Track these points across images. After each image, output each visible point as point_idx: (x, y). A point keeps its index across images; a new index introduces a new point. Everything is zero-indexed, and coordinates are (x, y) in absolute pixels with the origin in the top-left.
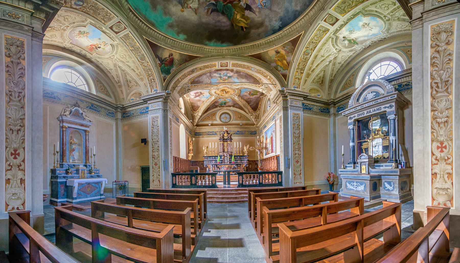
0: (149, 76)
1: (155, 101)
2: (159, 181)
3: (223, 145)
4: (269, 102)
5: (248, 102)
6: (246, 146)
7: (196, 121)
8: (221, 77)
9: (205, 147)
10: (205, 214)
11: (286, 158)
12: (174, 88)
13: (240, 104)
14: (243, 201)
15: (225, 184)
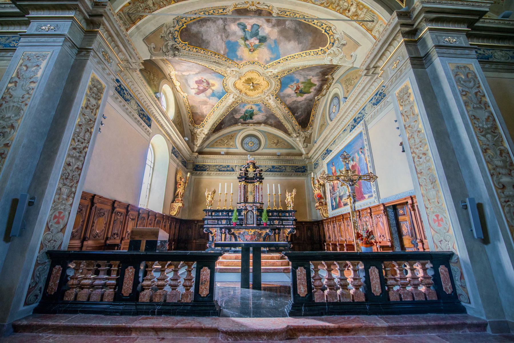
1: (53, 14)
6: (291, 191)
7: (199, 142)
15: (245, 284)
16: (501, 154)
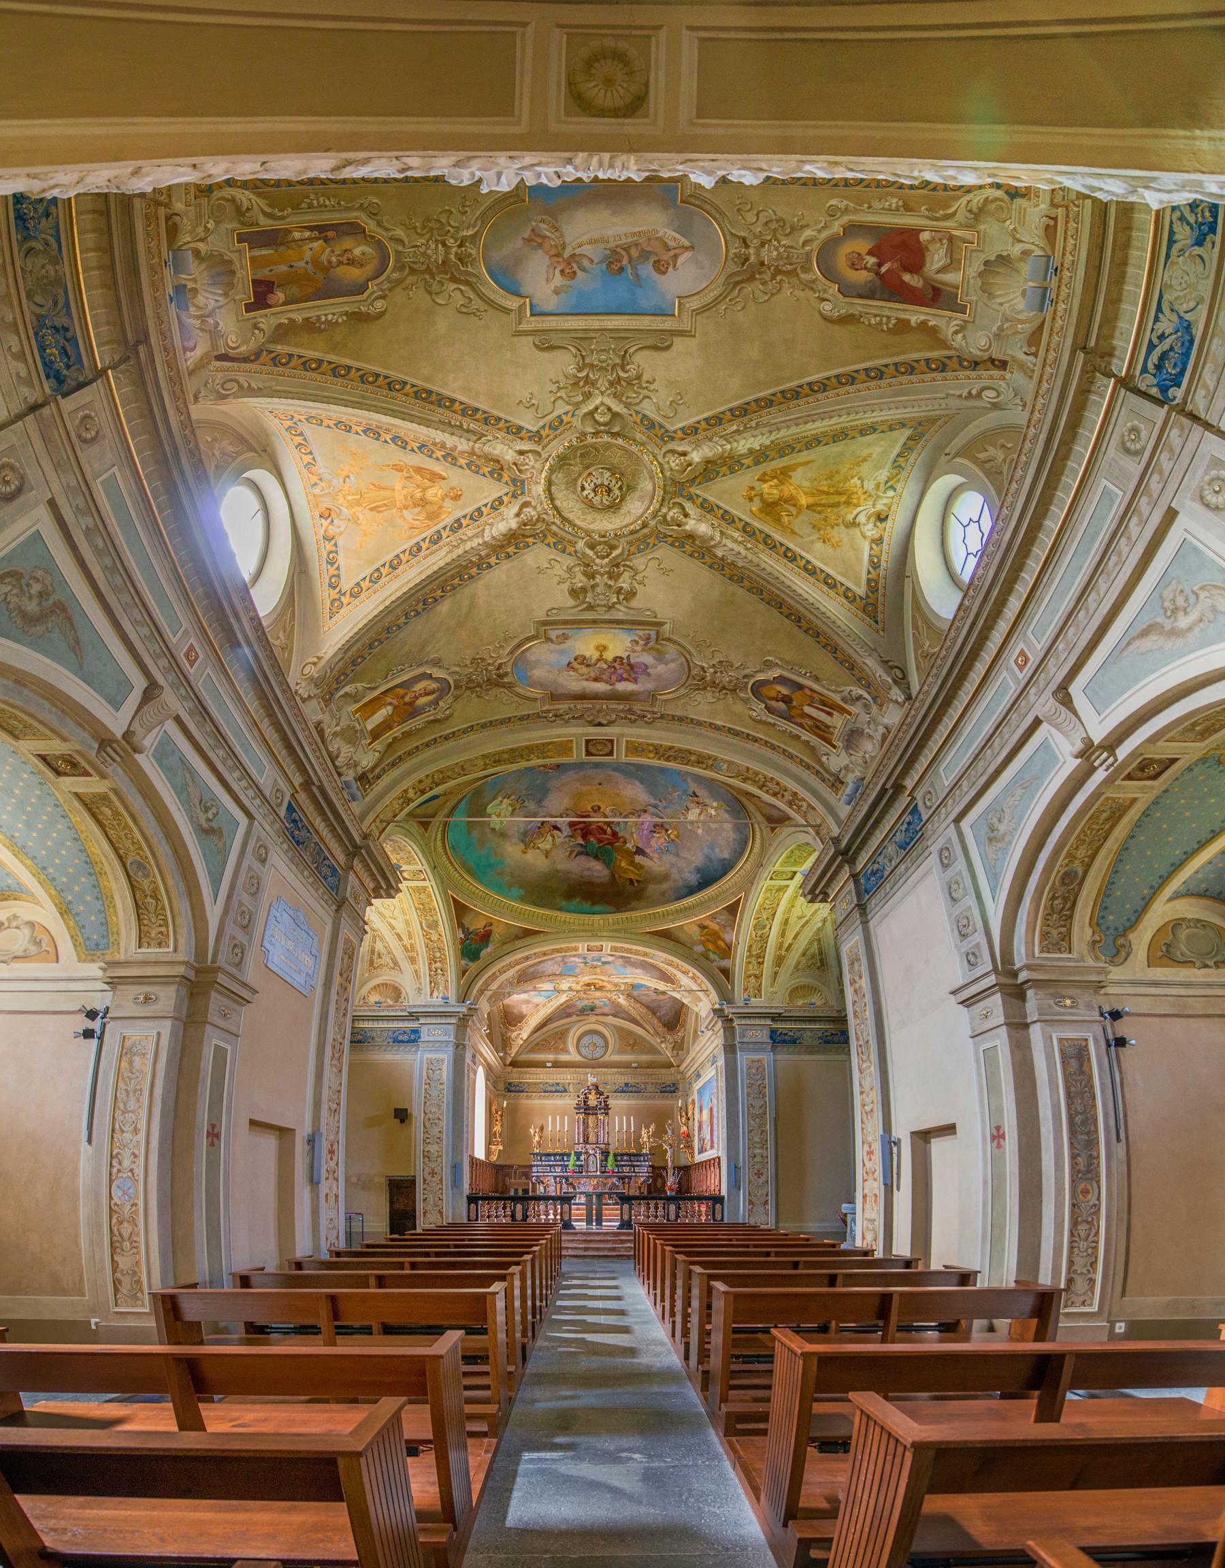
0: (432, 960)
2: (441, 1213)
5: (652, 1009)
6: (647, 1127)
12: (481, 992)
13: (633, 1012)
15: (589, 1222)
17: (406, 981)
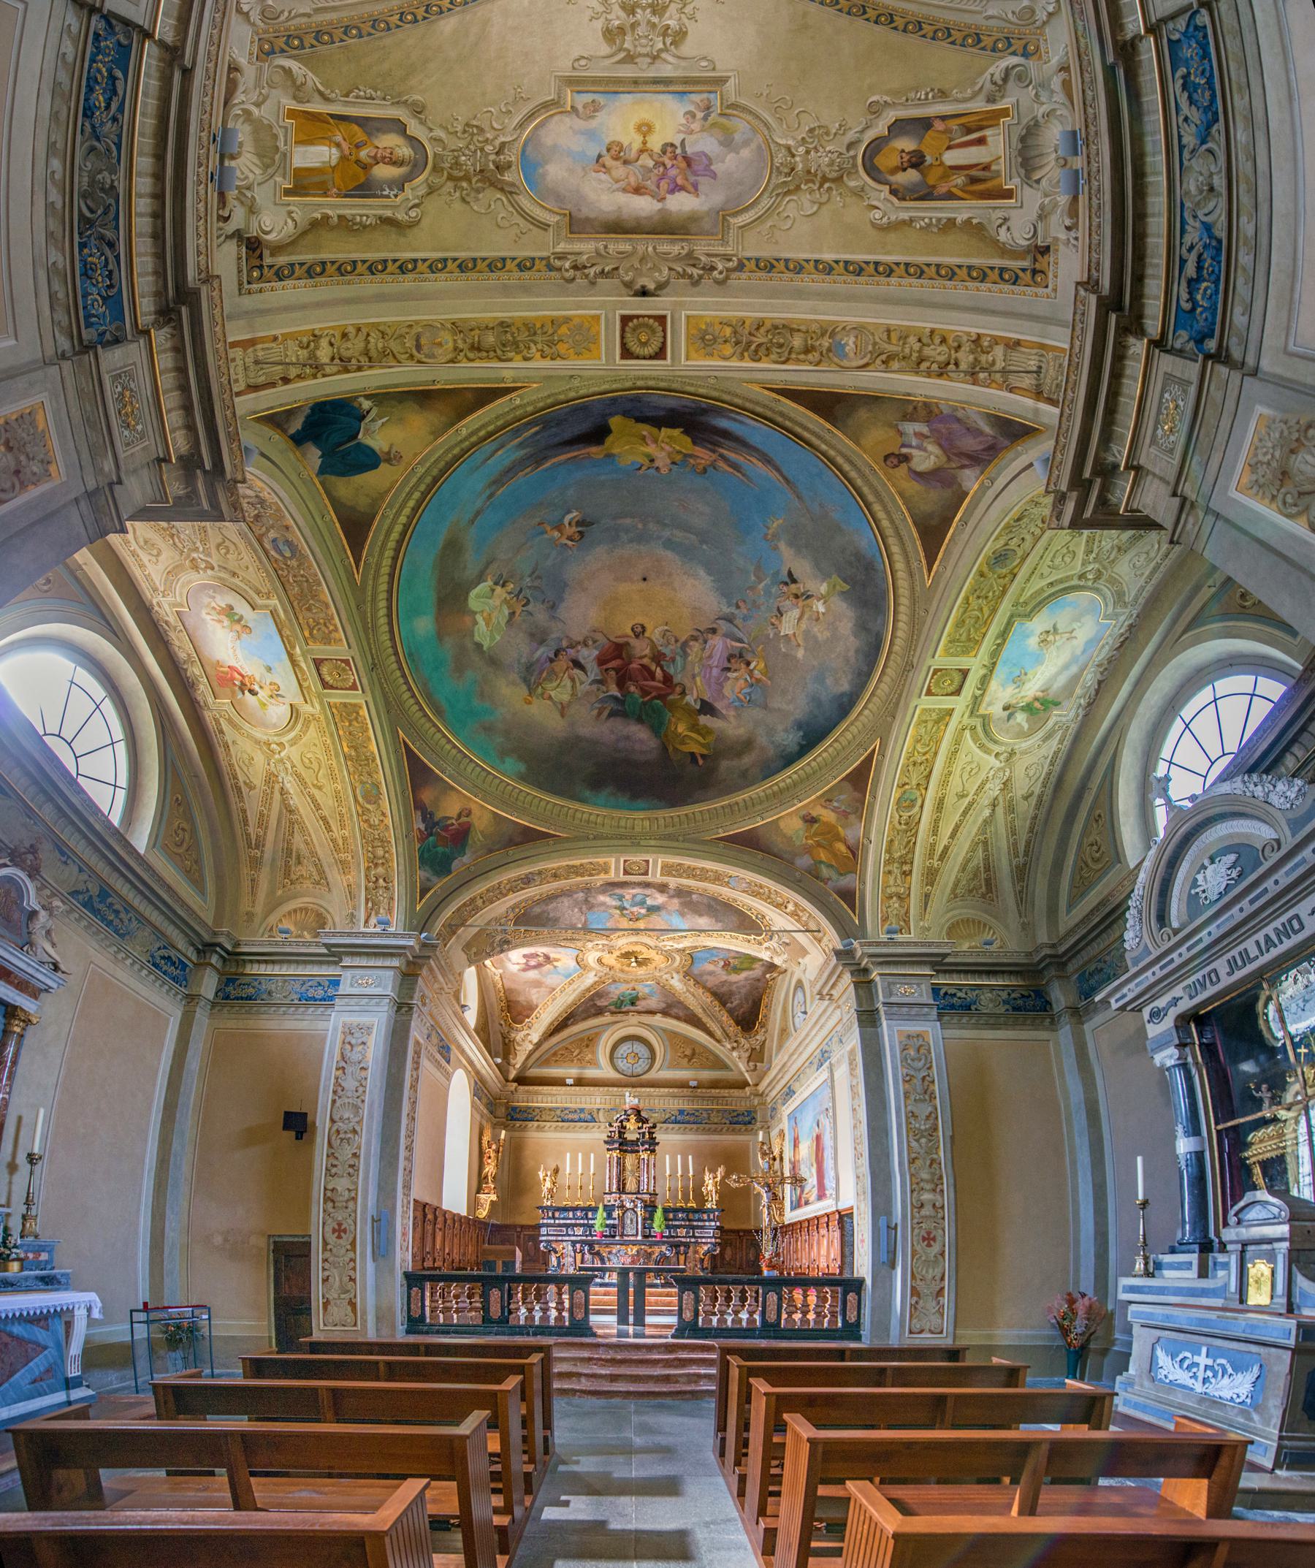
0: (374, 862)
2: (352, 1304)
3: (618, 1163)
4: (800, 994)
5: (721, 997)
6: (713, 1171)
7: (519, 1061)
8: (622, 908)
9: (545, 1169)
10: (546, 1439)
11: (883, 1222)
14: (693, 1393)
15: (623, 1320)
16: (931, 1165)
17: (336, 907)
